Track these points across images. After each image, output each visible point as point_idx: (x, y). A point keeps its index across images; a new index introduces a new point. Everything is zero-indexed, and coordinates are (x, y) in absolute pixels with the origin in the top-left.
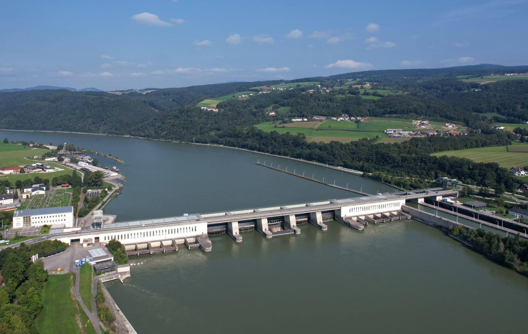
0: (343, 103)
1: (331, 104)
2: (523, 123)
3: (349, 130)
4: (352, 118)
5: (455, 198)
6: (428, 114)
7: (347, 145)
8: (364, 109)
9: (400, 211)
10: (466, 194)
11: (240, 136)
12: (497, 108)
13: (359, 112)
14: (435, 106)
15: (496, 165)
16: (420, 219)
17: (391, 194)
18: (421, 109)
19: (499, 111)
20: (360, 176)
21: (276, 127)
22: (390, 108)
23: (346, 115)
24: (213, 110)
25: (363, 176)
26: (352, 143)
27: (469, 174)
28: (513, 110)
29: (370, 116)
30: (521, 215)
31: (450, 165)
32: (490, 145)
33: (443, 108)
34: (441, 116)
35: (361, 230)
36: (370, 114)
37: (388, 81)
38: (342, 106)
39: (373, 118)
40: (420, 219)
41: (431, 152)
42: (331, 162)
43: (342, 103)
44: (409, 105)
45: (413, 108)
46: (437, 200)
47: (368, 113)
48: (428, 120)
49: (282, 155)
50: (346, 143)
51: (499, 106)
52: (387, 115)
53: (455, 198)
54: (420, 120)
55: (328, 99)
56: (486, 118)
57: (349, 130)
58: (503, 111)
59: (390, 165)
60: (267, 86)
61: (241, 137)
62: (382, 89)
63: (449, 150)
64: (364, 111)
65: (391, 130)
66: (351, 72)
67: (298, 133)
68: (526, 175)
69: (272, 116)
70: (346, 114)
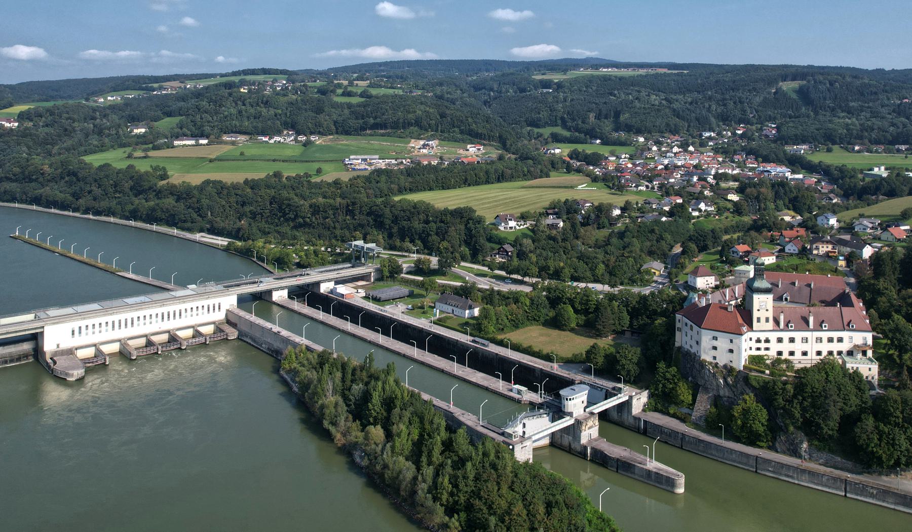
0: (289, 109)
1: (264, 110)
2: (591, 143)
3: (277, 160)
4: (302, 138)
5: (368, 283)
6: (439, 129)
7: (235, 186)
8: (326, 121)
9: (220, 324)
10: (387, 274)
11: (34, 177)
12: (562, 119)
13: (316, 125)
14: (454, 115)
15: (470, 210)
16: (251, 338)
17: (217, 285)
18: (428, 120)
19: (565, 126)
20: (223, 250)
21: (130, 156)
22: (375, 118)
23: (290, 133)
24: (4, 125)
25: (227, 249)
26: (246, 182)
27: (421, 232)
28: (583, 122)
29: (337, 133)
30: (452, 307)
31: (393, 216)
32: (512, 178)
33: (466, 117)
34: (462, 132)
35: (73, 379)
36: (337, 129)
37: (420, 78)
38: (286, 114)
39: (342, 137)
40: (251, 338)
41: (391, 195)
42: (189, 225)
43: (287, 109)
44: (409, 112)
45: (414, 118)
46: (322, 291)
47: (333, 128)
48: (439, 140)
49: (105, 215)
50: (233, 182)
51: (565, 116)
52: (368, 132)
53: (368, 283)
54: (424, 139)
55: (262, 101)
56: (541, 135)
57: (277, 160)
58: (569, 124)
59: (292, 224)
60: (180, 82)
61: (36, 180)
62: (387, 88)
63: (431, 189)
64: (325, 123)
65: (358, 157)
66: (367, 62)
67: (151, 166)
68: (518, 228)
69: (138, 136)
70: (290, 131)
